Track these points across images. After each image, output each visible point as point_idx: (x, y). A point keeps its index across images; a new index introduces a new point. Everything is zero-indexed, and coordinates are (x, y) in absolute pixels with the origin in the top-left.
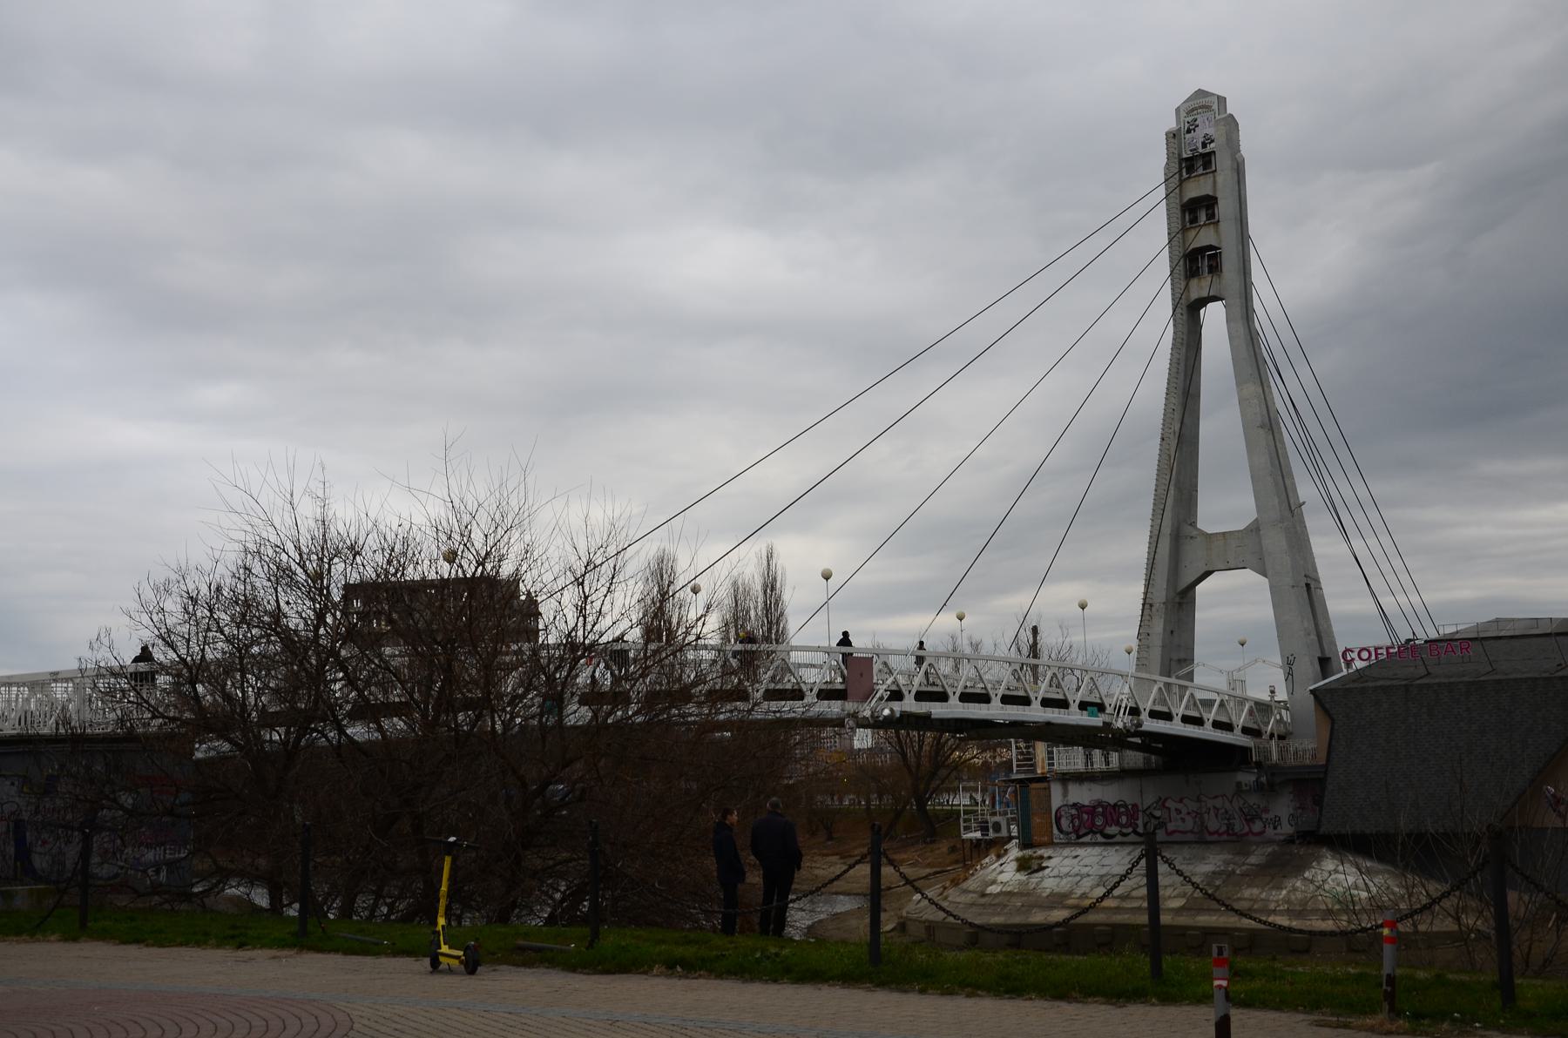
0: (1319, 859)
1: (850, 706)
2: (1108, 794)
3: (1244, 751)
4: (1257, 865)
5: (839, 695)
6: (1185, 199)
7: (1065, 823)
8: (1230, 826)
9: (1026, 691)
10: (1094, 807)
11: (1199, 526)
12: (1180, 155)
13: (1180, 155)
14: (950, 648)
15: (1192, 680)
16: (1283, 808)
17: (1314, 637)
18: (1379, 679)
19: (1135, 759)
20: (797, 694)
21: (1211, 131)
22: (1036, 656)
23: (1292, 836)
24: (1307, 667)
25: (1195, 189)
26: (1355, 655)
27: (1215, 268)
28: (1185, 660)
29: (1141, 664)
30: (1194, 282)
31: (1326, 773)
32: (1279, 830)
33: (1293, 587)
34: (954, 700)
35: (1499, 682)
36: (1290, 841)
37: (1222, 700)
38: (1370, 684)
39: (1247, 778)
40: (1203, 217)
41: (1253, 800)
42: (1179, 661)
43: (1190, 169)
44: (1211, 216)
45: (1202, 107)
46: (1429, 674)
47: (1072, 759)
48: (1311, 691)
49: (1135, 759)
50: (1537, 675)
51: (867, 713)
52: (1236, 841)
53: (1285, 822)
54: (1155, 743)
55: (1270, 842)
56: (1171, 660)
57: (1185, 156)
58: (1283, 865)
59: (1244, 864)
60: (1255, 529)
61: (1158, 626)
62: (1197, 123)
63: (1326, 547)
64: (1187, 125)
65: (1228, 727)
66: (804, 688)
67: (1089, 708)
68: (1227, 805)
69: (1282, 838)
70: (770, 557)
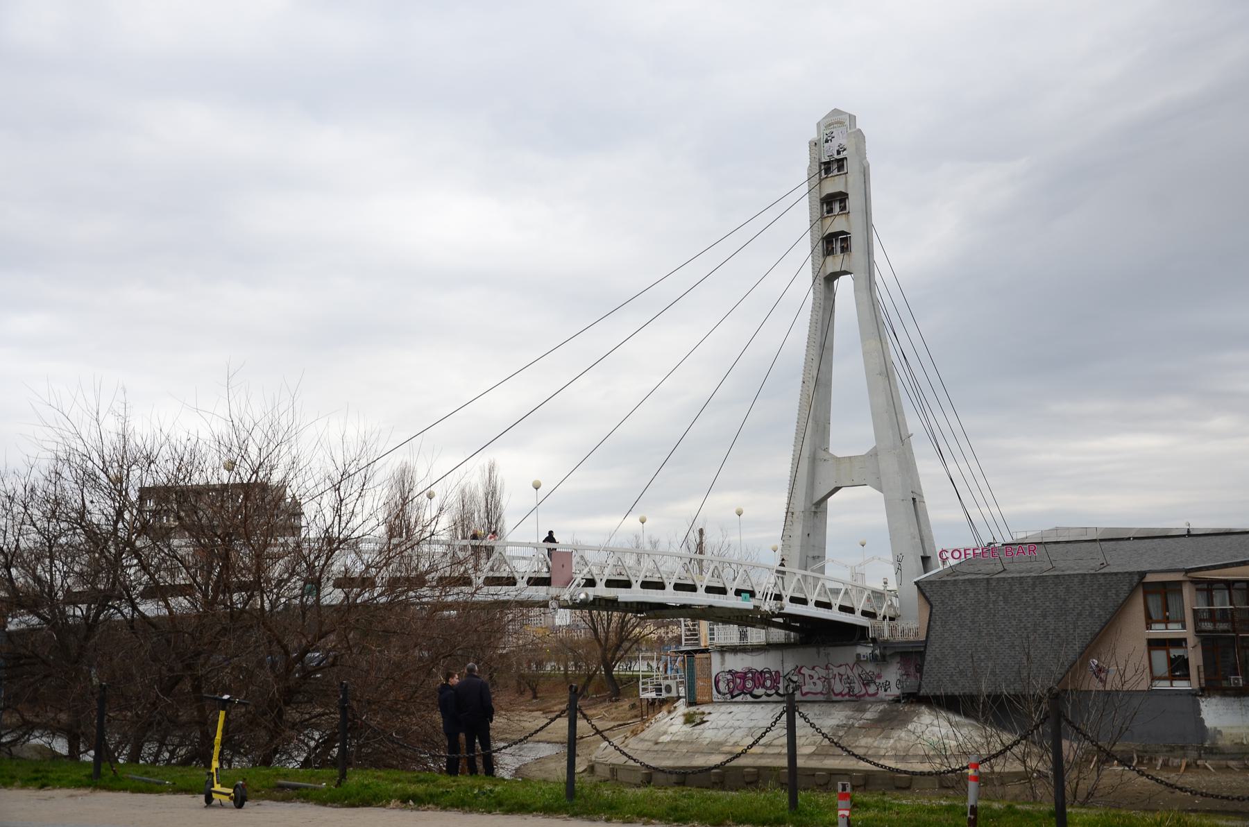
0: (919, 715)
2: (758, 662)
3: (864, 629)
6: (823, 195)
7: (722, 686)
10: (746, 673)
11: (831, 451)
14: (634, 545)
15: (824, 574)
19: (778, 635)
21: (844, 142)
22: (701, 553)
23: (898, 697)
26: (949, 555)
27: (845, 249)
30: (829, 259)
31: (925, 647)
34: (636, 587)
36: (897, 700)
39: (865, 651)
40: (837, 207)
41: (870, 668)
43: (828, 171)
44: (843, 208)
45: (837, 123)
46: (1005, 570)
47: (729, 634)
49: (778, 635)
52: (856, 700)
55: (882, 701)
57: (824, 160)
58: (889, 720)
59: (861, 719)
60: (874, 454)
62: (833, 135)
64: (825, 135)
67: (742, 594)
68: (849, 672)
69: (891, 698)
70: (491, 470)
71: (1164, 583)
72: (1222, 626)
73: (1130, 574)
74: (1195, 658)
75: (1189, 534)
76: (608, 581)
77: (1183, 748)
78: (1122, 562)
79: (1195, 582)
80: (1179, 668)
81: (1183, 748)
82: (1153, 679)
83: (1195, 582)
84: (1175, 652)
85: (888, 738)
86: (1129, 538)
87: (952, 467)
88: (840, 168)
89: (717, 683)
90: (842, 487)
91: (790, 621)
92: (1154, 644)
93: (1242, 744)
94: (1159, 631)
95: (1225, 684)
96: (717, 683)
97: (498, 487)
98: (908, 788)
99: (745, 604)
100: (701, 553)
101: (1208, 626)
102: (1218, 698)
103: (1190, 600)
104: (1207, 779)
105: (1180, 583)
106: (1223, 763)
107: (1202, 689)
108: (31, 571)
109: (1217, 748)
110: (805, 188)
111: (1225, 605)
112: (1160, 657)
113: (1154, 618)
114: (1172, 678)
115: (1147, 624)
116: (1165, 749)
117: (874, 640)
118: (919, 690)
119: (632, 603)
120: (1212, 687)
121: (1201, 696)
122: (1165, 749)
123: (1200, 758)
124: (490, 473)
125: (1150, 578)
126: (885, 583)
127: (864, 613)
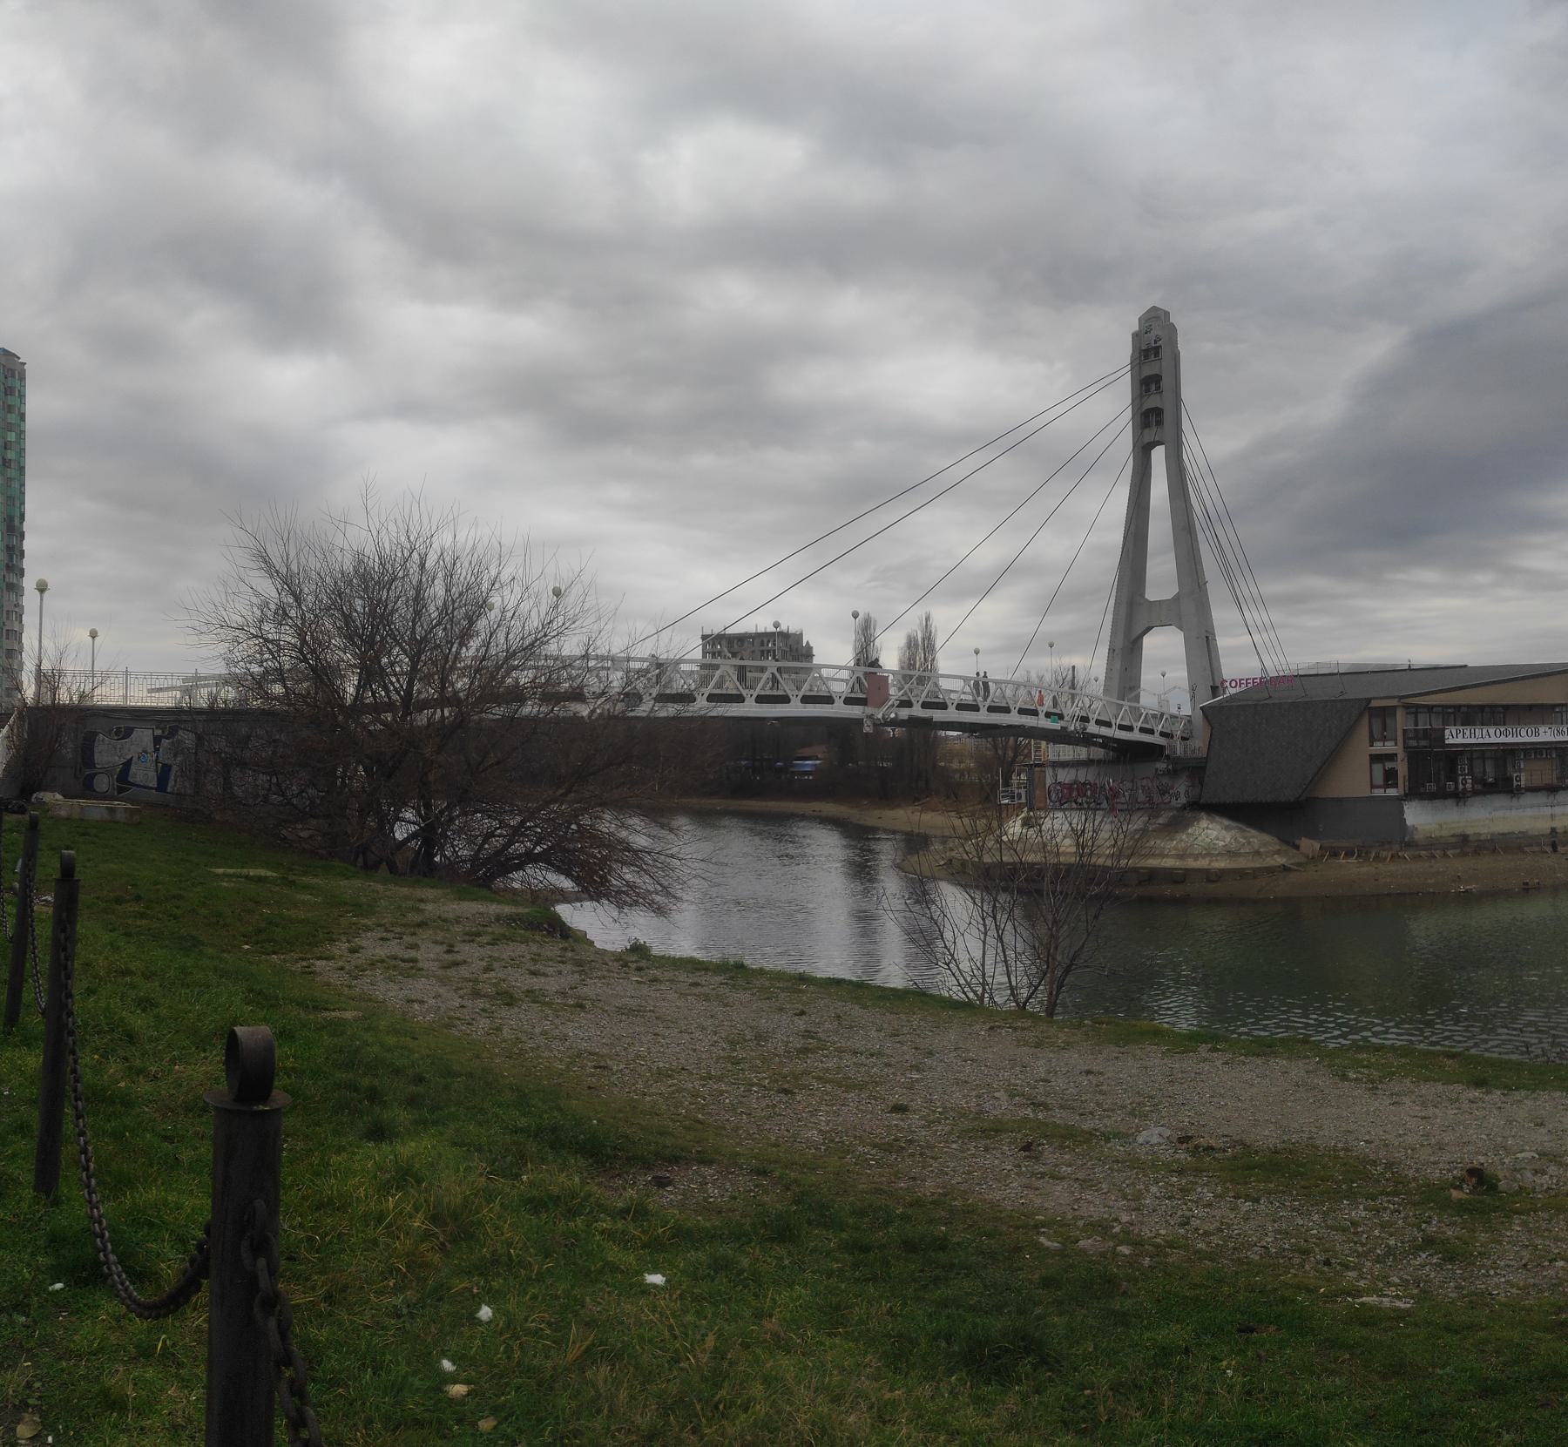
0: (1198, 820)
1: (869, 710)
2: (1082, 775)
3: (1162, 747)
4: (1163, 824)
5: (862, 702)
6: (1142, 377)
7: (1054, 797)
8: (1151, 799)
9: (785, 691)
10: (1072, 784)
11: (1146, 596)
12: (1140, 347)
13: (1140, 347)
14: (1026, 678)
15: (1139, 702)
16: (1181, 787)
17: (1209, 672)
18: (1243, 700)
19: (1098, 753)
20: (943, 706)
21: (1160, 333)
22: (1074, 689)
23: (1185, 804)
24: (1204, 691)
25: (1149, 370)
26: (1228, 684)
27: (1159, 423)
28: (1134, 687)
29: (1106, 690)
30: (1146, 431)
31: (1206, 762)
32: (1179, 801)
33: (1198, 638)
34: (1014, 713)
35: (1307, 702)
36: (1184, 808)
37: (1147, 714)
38: (1235, 704)
39: (1161, 766)
40: (1153, 387)
41: (1165, 780)
42: (1130, 688)
43: (1146, 357)
44: (1158, 388)
46: (1270, 697)
47: (1067, 752)
48: (1201, 708)
49: (1098, 753)
50: (1327, 698)
51: (880, 716)
52: (1153, 809)
53: (1182, 796)
54: (960, 735)
55: (1171, 809)
56: (1125, 688)
57: (1143, 348)
58: (1178, 824)
59: (1155, 823)
60: (1177, 599)
61: (1118, 665)
63: (1222, 615)
65: (1151, 732)
66: (948, 702)
68: (1150, 785)
69: (1180, 806)
70: (928, 619)
71: (1384, 708)
72: (1423, 743)
73: (1359, 700)
74: (1402, 768)
75: (1410, 669)
76: (958, 704)
77: (1390, 843)
78: (1356, 692)
79: (1407, 707)
80: (1390, 778)
81: (1390, 843)
82: (1373, 787)
83: (1407, 707)
84: (1389, 765)
85: (1173, 840)
86: (1368, 672)
87: (1247, 614)
88: (1157, 354)
89: (1049, 793)
90: (1153, 627)
91: (1107, 742)
92: (1376, 758)
93: (1431, 837)
94: (1379, 748)
95: (1422, 790)
96: (1049, 793)
97: (933, 631)
98: (1183, 882)
99: (1056, 725)
100: (1074, 689)
101: (1413, 743)
102: (1417, 801)
103: (1402, 722)
104: (1403, 867)
105: (1394, 708)
106: (1417, 853)
107: (1406, 795)
108: (402, 693)
109: (1413, 842)
110: (1129, 367)
111: (1426, 725)
112: (1378, 769)
113: (1376, 737)
114: (1386, 786)
115: (1370, 741)
116: (1377, 844)
117: (1168, 757)
118: (1200, 799)
119: (965, 723)
120: (1415, 792)
121: (1405, 800)
122: (1377, 844)
123: (1401, 850)
124: (926, 622)
125: (1374, 704)
126: (1179, 708)
127: (1162, 734)
